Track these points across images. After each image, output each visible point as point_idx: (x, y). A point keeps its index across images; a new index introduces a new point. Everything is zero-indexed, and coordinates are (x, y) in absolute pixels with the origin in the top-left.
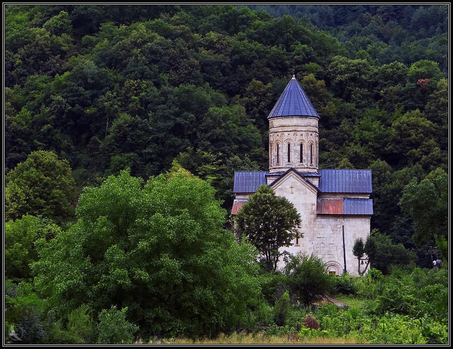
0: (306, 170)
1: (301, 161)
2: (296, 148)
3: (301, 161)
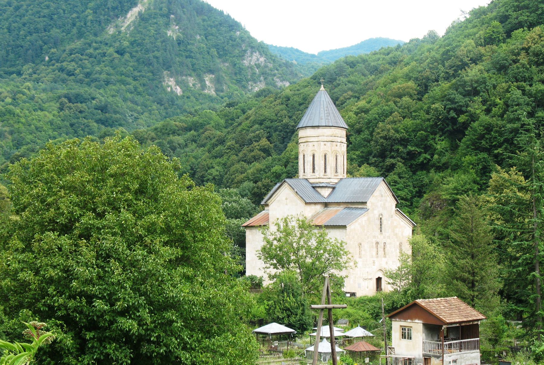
0: (317, 181)
1: (314, 172)
2: (320, 163)
3: (314, 172)
